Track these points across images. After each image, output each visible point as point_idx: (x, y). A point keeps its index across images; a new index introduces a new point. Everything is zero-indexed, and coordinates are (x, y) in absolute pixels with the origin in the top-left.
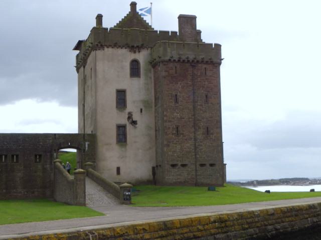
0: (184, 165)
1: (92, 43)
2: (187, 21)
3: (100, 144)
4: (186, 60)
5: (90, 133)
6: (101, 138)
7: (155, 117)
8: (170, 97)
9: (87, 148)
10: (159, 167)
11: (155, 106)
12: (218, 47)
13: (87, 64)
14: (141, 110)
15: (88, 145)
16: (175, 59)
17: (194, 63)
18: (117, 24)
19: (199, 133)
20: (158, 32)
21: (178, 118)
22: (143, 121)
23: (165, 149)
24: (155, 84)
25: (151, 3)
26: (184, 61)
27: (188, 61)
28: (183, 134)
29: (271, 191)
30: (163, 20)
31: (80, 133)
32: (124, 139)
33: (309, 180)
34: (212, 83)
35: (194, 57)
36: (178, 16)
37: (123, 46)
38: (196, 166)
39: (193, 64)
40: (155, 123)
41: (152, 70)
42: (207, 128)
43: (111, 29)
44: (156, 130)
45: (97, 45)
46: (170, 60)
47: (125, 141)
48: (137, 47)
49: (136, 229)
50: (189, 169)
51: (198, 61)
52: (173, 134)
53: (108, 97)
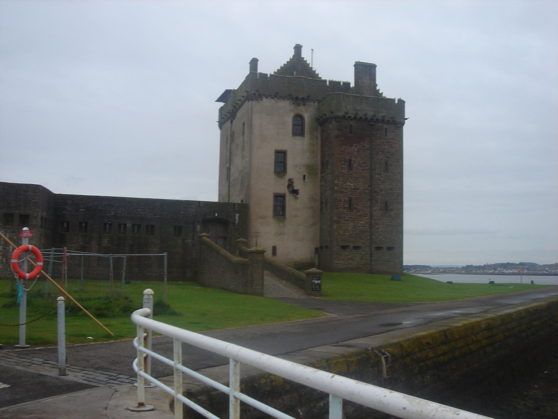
0: (356, 248)
1: (247, 92)
2: (365, 71)
4: (364, 117)
5: (239, 202)
7: (321, 186)
8: (343, 163)
9: (237, 222)
11: (322, 173)
12: (402, 103)
13: (236, 118)
14: (304, 176)
15: (239, 217)
16: (350, 115)
19: (375, 208)
20: (328, 83)
21: (352, 189)
22: (306, 190)
23: (335, 226)
24: (323, 146)
25: (312, 50)
26: (361, 118)
27: (366, 119)
28: (356, 208)
29: (495, 283)
30: (333, 67)
31: (222, 201)
32: (281, 212)
33: (431, 268)
34: (394, 148)
35: (373, 114)
37: (286, 97)
39: (371, 123)
40: (321, 194)
41: (319, 128)
42: (386, 203)
43: (271, 75)
44: (322, 203)
45: (254, 94)
46: (344, 116)
47: (284, 214)
48: (303, 99)
49: (421, 342)
51: (378, 120)
52: (345, 208)
53: (264, 159)
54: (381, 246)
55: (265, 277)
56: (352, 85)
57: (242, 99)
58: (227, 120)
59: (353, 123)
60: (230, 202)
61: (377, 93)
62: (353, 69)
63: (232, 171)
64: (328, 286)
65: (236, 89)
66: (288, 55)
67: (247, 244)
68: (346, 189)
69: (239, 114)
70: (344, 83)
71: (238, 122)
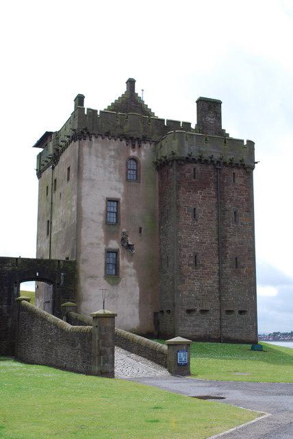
0: (204, 312)
2: (209, 108)
3: (82, 276)
4: (210, 159)
5: (64, 259)
6: (84, 268)
10: (166, 314)
13: (60, 162)
17: (218, 165)
18: (109, 106)
25: (143, 90)
26: (206, 161)
27: (212, 161)
28: (203, 265)
30: (172, 104)
31: (39, 258)
36: (196, 99)
38: (221, 312)
45: (82, 132)
50: (212, 318)
51: (225, 163)
52: (189, 265)
53: (94, 207)
54: (232, 309)
55: (116, 353)
56: (193, 126)
57: (67, 139)
58: (48, 166)
59: (198, 167)
60: (52, 258)
61: (222, 133)
62: (195, 106)
63: (54, 224)
64: (196, 363)
65: (58, 129)
66: (118, 91)
67: (76, 309)
68: (191, 242)
69: (62, 159)
70: (184, 123)
71: (61, 167)
